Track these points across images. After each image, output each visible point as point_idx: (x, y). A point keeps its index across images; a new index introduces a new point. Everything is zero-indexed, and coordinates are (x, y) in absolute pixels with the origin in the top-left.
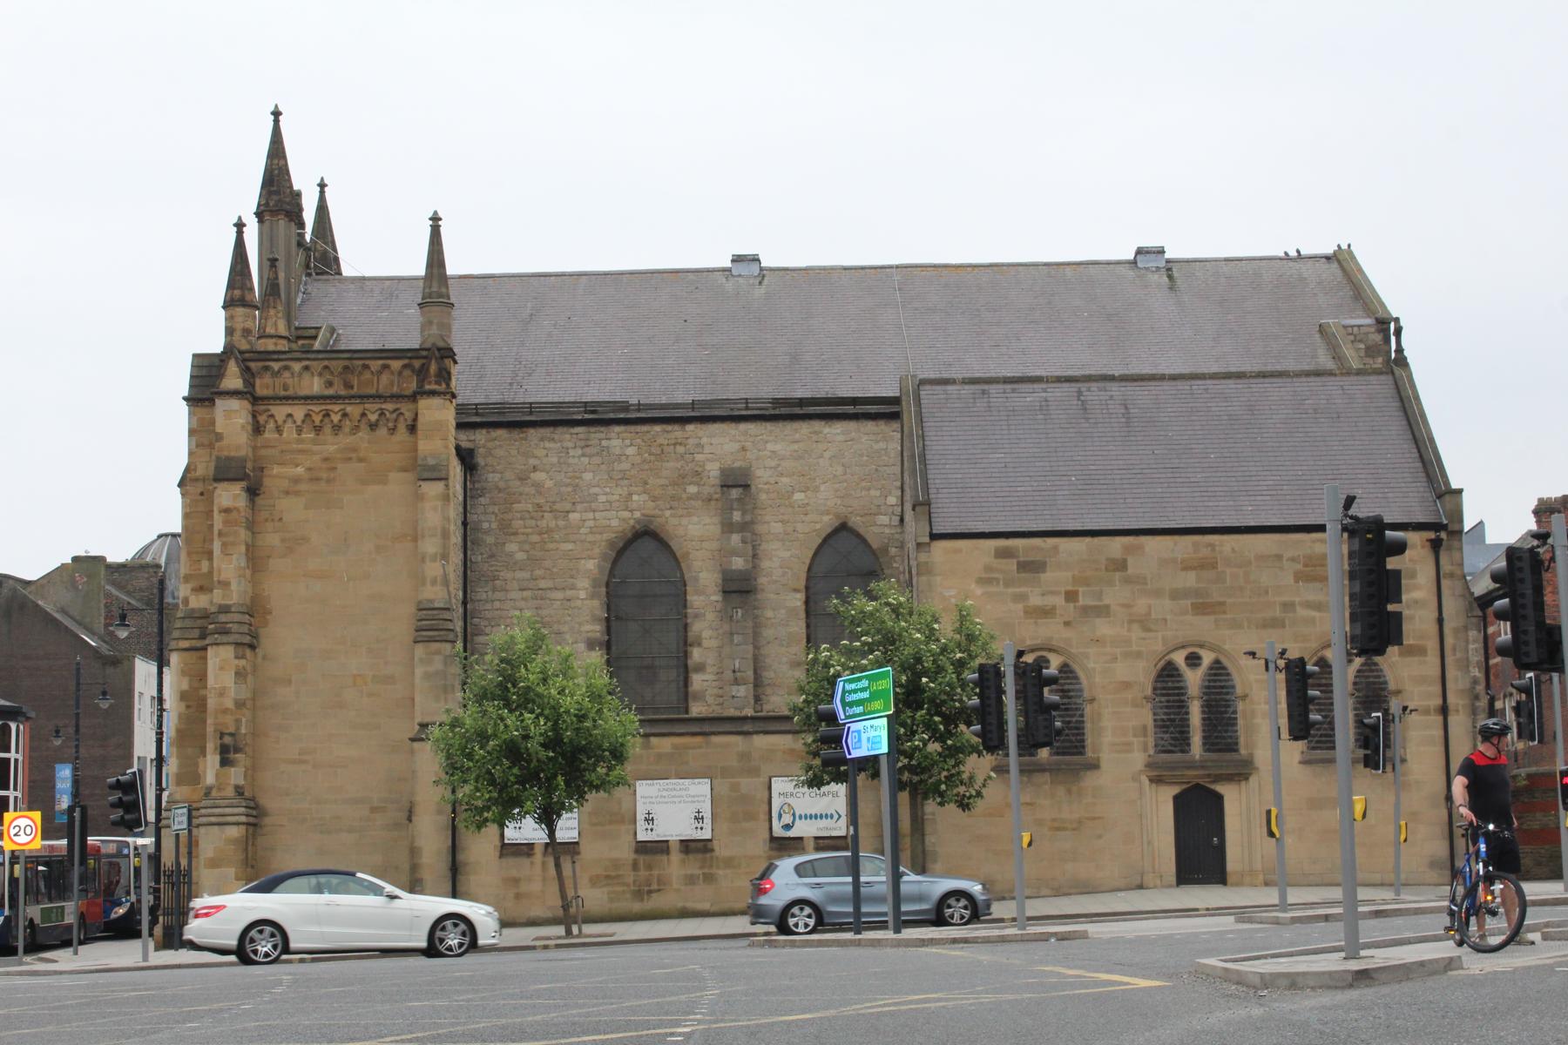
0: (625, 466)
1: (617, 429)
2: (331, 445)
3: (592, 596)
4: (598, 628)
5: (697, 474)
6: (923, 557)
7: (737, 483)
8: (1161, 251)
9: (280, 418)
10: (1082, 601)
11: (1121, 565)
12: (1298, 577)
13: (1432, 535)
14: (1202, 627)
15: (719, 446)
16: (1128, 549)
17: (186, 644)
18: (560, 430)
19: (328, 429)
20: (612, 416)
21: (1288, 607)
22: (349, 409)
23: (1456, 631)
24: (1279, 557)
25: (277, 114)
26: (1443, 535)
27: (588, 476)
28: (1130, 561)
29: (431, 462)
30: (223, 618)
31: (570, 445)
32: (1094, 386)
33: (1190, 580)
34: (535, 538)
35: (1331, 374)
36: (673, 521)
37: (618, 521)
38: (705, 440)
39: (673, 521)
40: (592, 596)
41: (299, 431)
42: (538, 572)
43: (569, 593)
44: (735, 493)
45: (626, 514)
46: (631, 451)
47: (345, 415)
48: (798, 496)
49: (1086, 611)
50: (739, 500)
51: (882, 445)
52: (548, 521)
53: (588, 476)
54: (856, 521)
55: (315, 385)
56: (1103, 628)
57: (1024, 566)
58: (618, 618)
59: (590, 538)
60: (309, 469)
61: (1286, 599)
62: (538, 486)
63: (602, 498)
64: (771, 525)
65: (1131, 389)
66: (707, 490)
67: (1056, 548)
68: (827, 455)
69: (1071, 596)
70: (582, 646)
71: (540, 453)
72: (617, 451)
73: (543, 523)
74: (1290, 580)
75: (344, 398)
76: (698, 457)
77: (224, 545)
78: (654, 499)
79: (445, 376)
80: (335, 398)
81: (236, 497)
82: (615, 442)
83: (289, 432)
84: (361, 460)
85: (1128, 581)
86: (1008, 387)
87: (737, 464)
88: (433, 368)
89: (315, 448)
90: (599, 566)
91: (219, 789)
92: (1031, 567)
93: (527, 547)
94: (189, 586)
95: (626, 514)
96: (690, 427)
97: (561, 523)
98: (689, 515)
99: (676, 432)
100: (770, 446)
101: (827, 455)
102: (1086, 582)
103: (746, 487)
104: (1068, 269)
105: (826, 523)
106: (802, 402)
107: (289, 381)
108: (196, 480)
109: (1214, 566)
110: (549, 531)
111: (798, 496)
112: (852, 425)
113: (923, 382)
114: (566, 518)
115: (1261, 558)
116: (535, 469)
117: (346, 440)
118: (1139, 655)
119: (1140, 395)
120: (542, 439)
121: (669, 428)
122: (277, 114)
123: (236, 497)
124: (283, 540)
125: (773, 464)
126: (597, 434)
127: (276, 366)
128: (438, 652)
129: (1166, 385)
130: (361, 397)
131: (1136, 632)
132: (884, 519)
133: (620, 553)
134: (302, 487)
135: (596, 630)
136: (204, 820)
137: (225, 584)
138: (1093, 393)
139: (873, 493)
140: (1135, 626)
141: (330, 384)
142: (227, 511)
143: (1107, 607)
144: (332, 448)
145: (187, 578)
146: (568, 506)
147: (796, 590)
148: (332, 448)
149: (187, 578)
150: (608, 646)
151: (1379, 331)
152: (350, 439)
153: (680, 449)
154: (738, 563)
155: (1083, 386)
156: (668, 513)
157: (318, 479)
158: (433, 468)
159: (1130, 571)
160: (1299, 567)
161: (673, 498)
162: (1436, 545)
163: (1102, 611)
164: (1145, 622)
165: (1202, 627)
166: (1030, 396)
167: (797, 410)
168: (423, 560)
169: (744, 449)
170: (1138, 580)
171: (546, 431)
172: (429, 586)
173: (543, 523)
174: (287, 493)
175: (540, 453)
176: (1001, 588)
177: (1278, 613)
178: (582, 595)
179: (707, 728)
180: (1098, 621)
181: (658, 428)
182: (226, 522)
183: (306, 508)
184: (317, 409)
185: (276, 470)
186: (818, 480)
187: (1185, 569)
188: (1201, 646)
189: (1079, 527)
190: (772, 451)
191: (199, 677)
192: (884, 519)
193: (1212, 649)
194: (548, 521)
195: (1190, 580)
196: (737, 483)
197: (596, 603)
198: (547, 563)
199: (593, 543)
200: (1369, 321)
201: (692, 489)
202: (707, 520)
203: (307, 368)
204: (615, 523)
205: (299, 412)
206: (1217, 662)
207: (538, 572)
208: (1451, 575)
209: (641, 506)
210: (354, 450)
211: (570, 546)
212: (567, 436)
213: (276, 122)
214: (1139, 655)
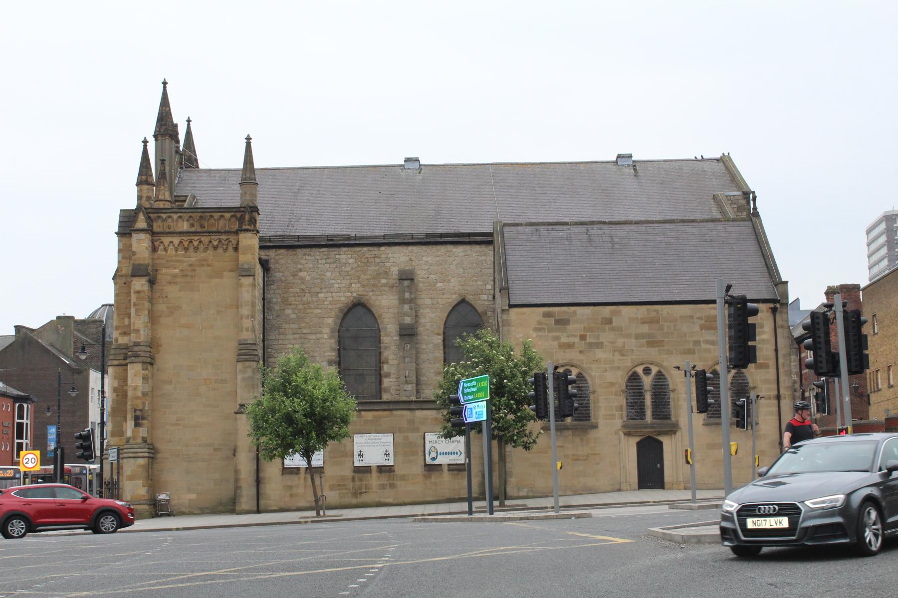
0: (348, 269)
1: (344, 249)
2: (193, 258)
3: (331, 337)
4: (334, 354)
6: (505, 317)
7: (407, 278)
8: (630, 156)
9: (166, 244)
11: (609, 321)
12: (702, 327)
13: (772, 305)
14: (652, 354)
15: (398, 258)
16: (612, 313)
17: (116, 362)
18: (314, 249)
19: (191, 249)
20: (341, 242)
21: (697, 343)
22: (203, 239)
23: (784, 356)
24: (692, 317)
25: (165, 83)
26: (778, 305)
28: (614, 318)
29: (246, 266)
30: (136, 349)
32: (595, 227)
33: (645, 329)
34: (301, 307)
35: (719, 220)
36: (374, 298)
37: (344, 298)
38: (390, 255)
39: (374, 298)
40: (331, 337)
41: (176, 250)
42: (302, 325)
43: (319, 336)
44: (406, 283)
45: (349, 294)
46: (351, 261)
47: (201, 242)
48: (439, 285)
49: (591, 345)
51: (484, 258)
52: (308, 298)
53: (329, 274)
54: (470, 298)
55: (185, 226)
56: (600, 354)
57: (558, 322)
58: (344, 349)
59: (329, 307)
61: (696, 339)
62: (302, 279)
63: (336, 286)
64: (425, 300)
65: (614, 229)
66: (391, 282)
67: (575, 312)
68: (454, 263)
69: (583, 338)
70: (325, 364)
72: (344, 261)
73: (305, 299)
76: (387, 264)
77: (137, 310)
78: (364, 286)
79: (253, 221)
81: (143, 285)
83: (171, 251)
84: (209, 266)
85: (613, 329)
88: (247, 217)
91: (134, 439)
92: (562, 322)
93: (296, 311)
94: (118, 332)
95: (349, 294)
96: (383, 248)
97: (314, 299)
98: (382, 295)
99: (375, 251)
100: (424, 259)
101: (454, 263)
102: (591, 330)
103: (412, 280)
104: (581, 166)
105: (454, 299)
107: (171, 224)
108: (122, 276)
109: (658, 321)
110: (308, 303)
111: (439, 285)
112: (467, 247)
113: (505, 225)
116: (301, 270)
117: (201, 255)
118: (618, 368)
120: (305, 255)
121: (371, 249)
122: (165, 83)
124: (168, 308)
125: (426, 268)
126: (334, 252)
127: (164, 216)
128: (250, 367)
129: (633, 227)
130: (209, 232)
131: (617, 357)
132: (485, 297)
133: (346, 315)
134: (178, 280)
135: (333, 355)
137: (137, 331)
138: (595, 231)
140: (617, 353)
141: (192, 225)
142: (138, 292)
144: (194, 259)
145: (117, 328)
146: (318, 290)
147: (438, 334)
148: (194, 259)
149: (117, 328)
150: (339, 364)
152: (203, 255)
153: (377, 260)
155: (589, 227)
156: (371, 294)
160: (703, 322)
161: (374, 285)
162: (774, 311)
163: (600, 345)
164: (622, 352)
165: (652, 354)
166: (562, 232)
167: (439, 240)
168: (242, 318)
169: (411, 260)
172: (245, 333)
173: (305, 299)
174: (170, 283)
176: (546, 333)
177: (691, 346)
178: (326, 336)
179: (391, 407)
181: (365, 249)
184: (185, 238)
185: (164, 271)
186: (449, 275)
187: (643, 323)
188: (651, 364)
190: (425, 260)
191: (124, 380)
193: (657, 365)
194: (308, 298)
195: (645, 329)
196: (407, 278)
197: (333, 341)
198: (307, 320)
199: (331, 309)
201: (384, 281)
202: (392, 297)
204: (343, 299)
205: (176, 240)
206: (660, 372)
207: (302, 325)
208: (782, 326)
209: (357, 290)
211: (319, 311)
212: (317, 253)
213: (165, 87)
214: (618, 368)
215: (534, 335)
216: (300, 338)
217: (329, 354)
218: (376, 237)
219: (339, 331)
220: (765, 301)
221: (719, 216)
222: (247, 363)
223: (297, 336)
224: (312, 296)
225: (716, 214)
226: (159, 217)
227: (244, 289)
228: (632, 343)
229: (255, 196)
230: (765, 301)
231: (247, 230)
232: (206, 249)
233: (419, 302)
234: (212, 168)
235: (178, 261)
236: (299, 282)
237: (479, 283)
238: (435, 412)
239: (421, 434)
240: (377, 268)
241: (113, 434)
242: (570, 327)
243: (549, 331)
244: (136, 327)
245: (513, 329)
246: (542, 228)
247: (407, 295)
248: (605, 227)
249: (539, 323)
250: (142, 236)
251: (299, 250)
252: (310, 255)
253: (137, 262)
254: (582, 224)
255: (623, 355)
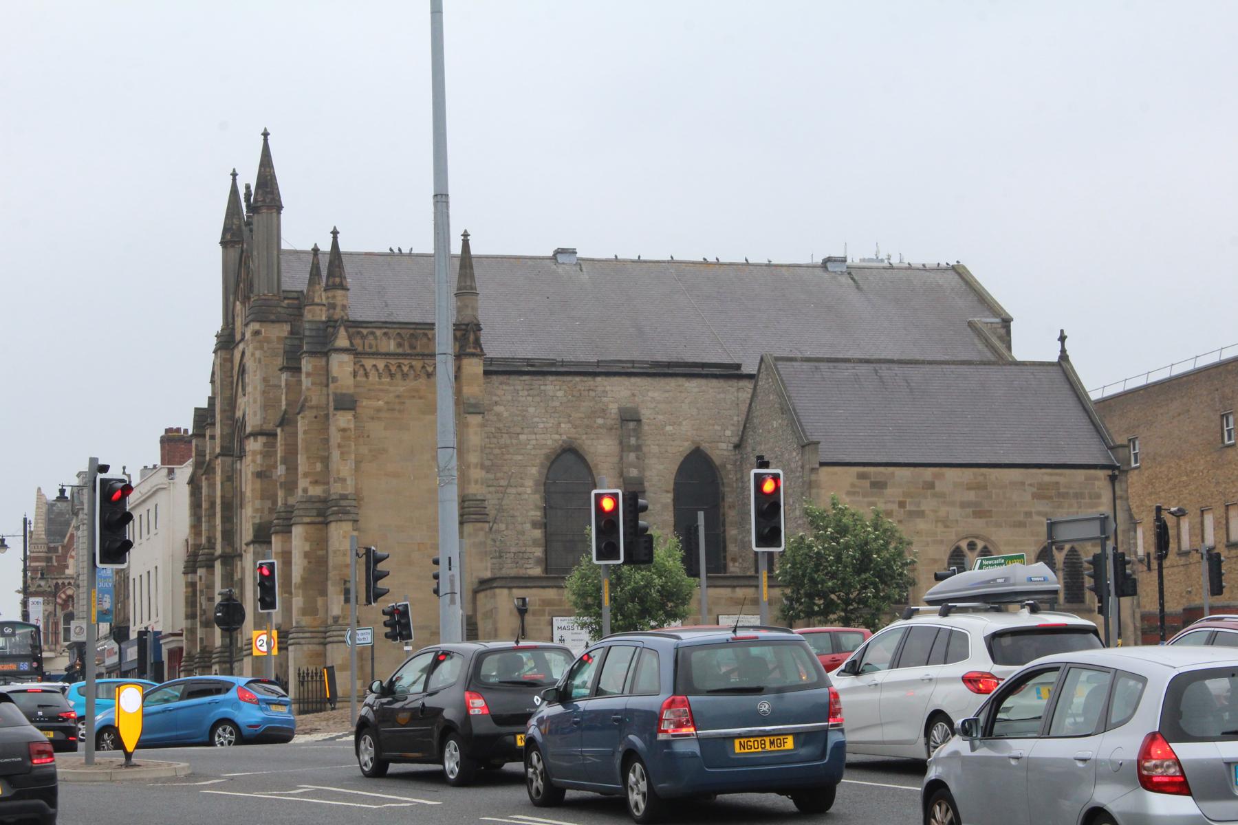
0: (557, 404)
1: (551, 378)
2: (401, 387)
4: (539, 514)
5: (603, 410)
6: (813, 477)
7: (630, 419)
8: (844, 260)
9: (368, 367)
10: (908, 508)
11: (931, 486)
12: (1034, 496)
13: (1110, 472)
14: (978, 525)
15: (618, 392)
16: (935, 476)
17: (307, 520)
18: (513, 377)
19: (399, 376)
20: (526, 369)
21: (1028, 514)
22: (414, 363)
23: (1123, 531)
24: (1023, 484)
25: (266, 134)
26: (1117, 473)
27: (532, 410)
28: (937, 483)
29: (472, 401)
30: (343, 503)
31: (519, 388)
32: (884, 366)
33: (971, 496)
34: (497, 451)
35: (994, 363)
36: (588, 442)
37: (552, 441)
38: (608, 388)
39: (588, 442)
40: (535, 492)
41: (380, 376)
42: (499, 475)
43: (520, 489)
44: (632, 425)
45: (557, 437)
46: (560, 394)
47: (411, 367)
48: (668, 428)
50: (634, 430)
51: (722, 396)
52: (505, 440)
53: (532, 410)
54: (705, 446)
55: (392, 346)
56: (921, 525)
57: (874, 485)
58: (551, 507)
59: (533, 452)
60: (387, 403)
61: (1026, 509)
62: (498, 415)
63: (541, 425)
64: (651, 448)
65: (907, 369)
66: (609, 422)
67: (893, 473)
68: (687, 401)
69: (902, 504)
70: (528, 526)
71: (500, 392)
72: (551, 394)
73: (502, 441)
74: (1028, 497)
75: (411, 355)
76: (604, 399)
77: (342, 453)
78: (576, 427)
80: (404, 355)
81: (349, 421)
82: (550, 387)
83: (373, 377)
84: (421, 398)
85: (935, 495)
86: (831, 364)
87: (629, 405)
88: (472, 338)
89: (392, 389)
90: (540, 473)
91: (344, 618)
92: (879, 485)
93: (491, 457)
94: (308, 480)
95: (557, 437)
96: (599, 379)
97: (514, 441)
98: (598, 438)
99: (589, 381)
101: (687, 401)
103: (639, 421)
104: (784, 270)
105: (685, 447)
106: (669, 365)
107: (373, 342)
108: (312, 408)
110: (506, 446)
111: (668, 428)
112: (702, 382)
113: (777, 359)
114: (517, 438)
115: (1013, 484)
116: (496, 403)
117: (412, 384)
118: (942, 542)
119: (915, 373)
120: (501, 383)
121: (585, 379)
122: (266, 134)
123: (349, 421)
124: (370, 451)
125: (653, 406)
126: (538, 381)
127: (365, 331)
128: (482, 529)
130: (423, 355)
131: (940, 528)
132: (723, 446)
133: (552, 463)
134: (383, 415)
135: (537, 514)
136: (336, 639)
137: (344, 480)
138: (884, 370)
139: (717, 427)
140: (939, 524)
141: (399, 345)
142: (344, 430)
143: (923, 512)
144: (402, 389)
145: (306, 475)
146: (519, 430)
147: (668, 492)
148: (402, 389)
149: (306, 475)
150: (545, 525)
151: (1004, 327)
154: (634, 473)
155: (877, 366)
156: (584, 437)
157: (393, 410)
158: (475, 406)
159: (937, 489)
160: (1035, 490)
161: (587, 426)
162: (1113, 479)
163: (921, 514)
164: (945, 522)
165: (978, 525)
166: (846, 372)
167: (666, 370)
168: (469, 467)
169: (633, 395)
170: (942, 495)
171: (501, 378)
172: (473, 485)
174: (373, 418)
175: (500, 392)
176: (860, 498)
177: (1021, 518)
178: (529, 491)
179: (544, 584)
180: (918, 520)
181: (578, 379)
182: (343, 438)
183: (385, 429)
184: (393, 362)
185: (365, 403)
186: (683, 419)
187: (969, 489)
188: (977, 537)
189: (885, 460)
190: (652, 397)
191: (321, 542)
192: (723, 446)
193: (982, 539)
194: (505, 440)
195: (971, 496)
196: (630, 419)
197: (537, 496)
198: (506, 469)
199: (535, 456)
200: (997, 320)
201: (600, 421)
202: (610, 442)
203: (385, 334)
204: (550, 442)
205: (381, 364)
206: (985, 547)
207: (499, 475)
208: (1121, 497)
209: (566, 431)
210: (417, 391)
211: (520, 457)
212: (518, 382)
213: (266, 140)
214: (942, 542)
215: (847, 499)
216: (497, 492)
217: (532, 513)
218: (588, 364)
219: (545, 484)
220: (1103, 467)
221: (993, 359)
222: (479, 525)
223: (491, 489)
224: (511, 438)
225: (989, 355)
226: (359, 333)
227: (471, 430)
228: (956, 513)
229: (475, 309)
230: (1103, 467)
231: (473, 355)
232: (417, 377)
233: (645, 449)
234: (298, 248)
235: (382, 390)
236: (495, 418)
237: (717, 427)
238: (729, 590)
239: (547, 618)
240: (591, 404)
241: (304, 612)
242: (888, 491)
243: (864, 496)
244: (341, 475)
245: (823, 491)
246: (822, 365)
247: (633, 441)
248: (895, 367)
249: (853, 485)
250: (346, 358)
251: (494, 377)
252: (508, 384)
253: (339, 391)
254: (867, 361)
255: (946, 526)
